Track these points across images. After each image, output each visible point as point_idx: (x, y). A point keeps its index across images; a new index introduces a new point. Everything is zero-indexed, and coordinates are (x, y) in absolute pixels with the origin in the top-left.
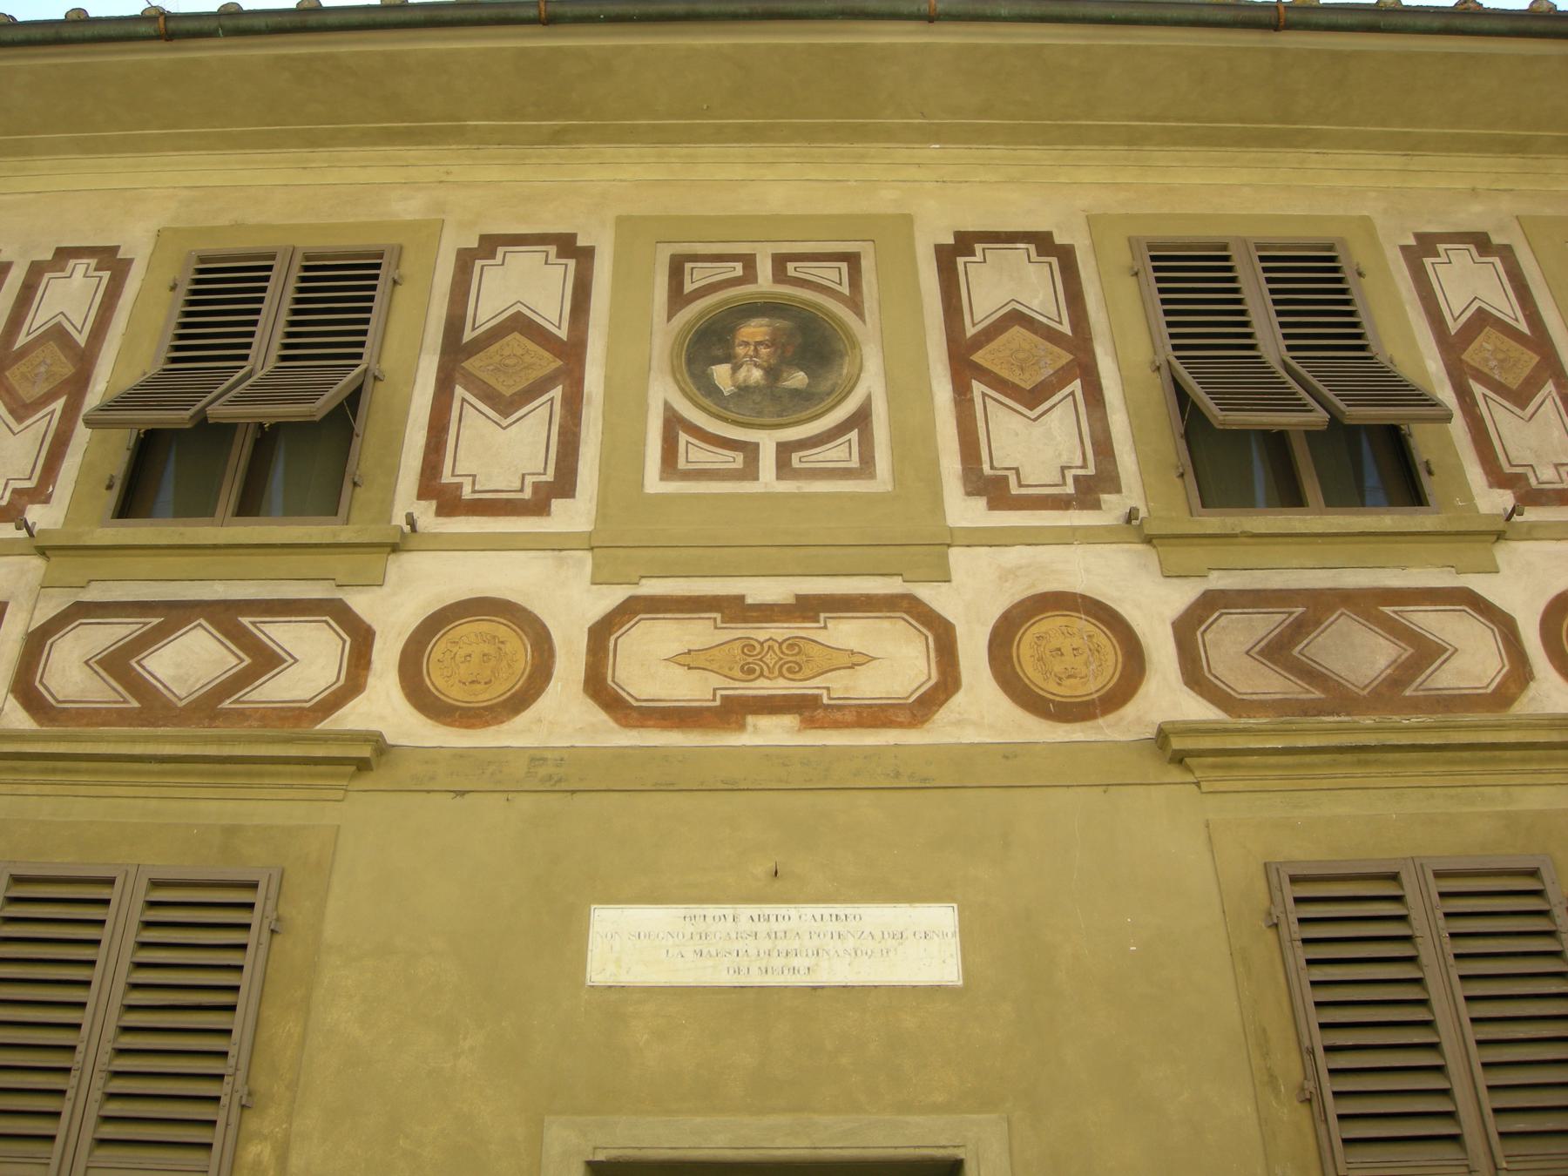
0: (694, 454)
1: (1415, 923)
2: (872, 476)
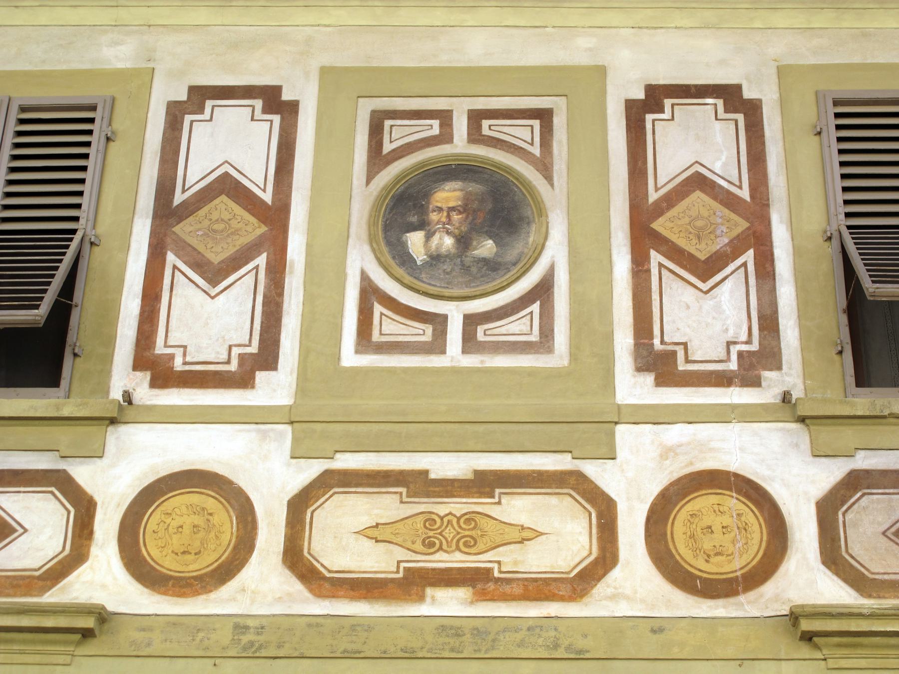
0: (389, 326)
2: (550, 350)
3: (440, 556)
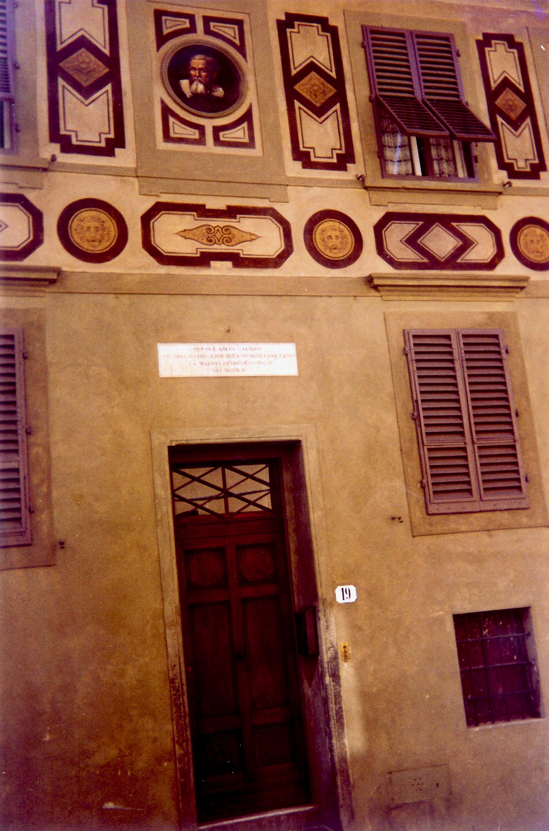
0: (178, 129)
1: (454, 355)
2: (204, 144)
3: (216, 246)
